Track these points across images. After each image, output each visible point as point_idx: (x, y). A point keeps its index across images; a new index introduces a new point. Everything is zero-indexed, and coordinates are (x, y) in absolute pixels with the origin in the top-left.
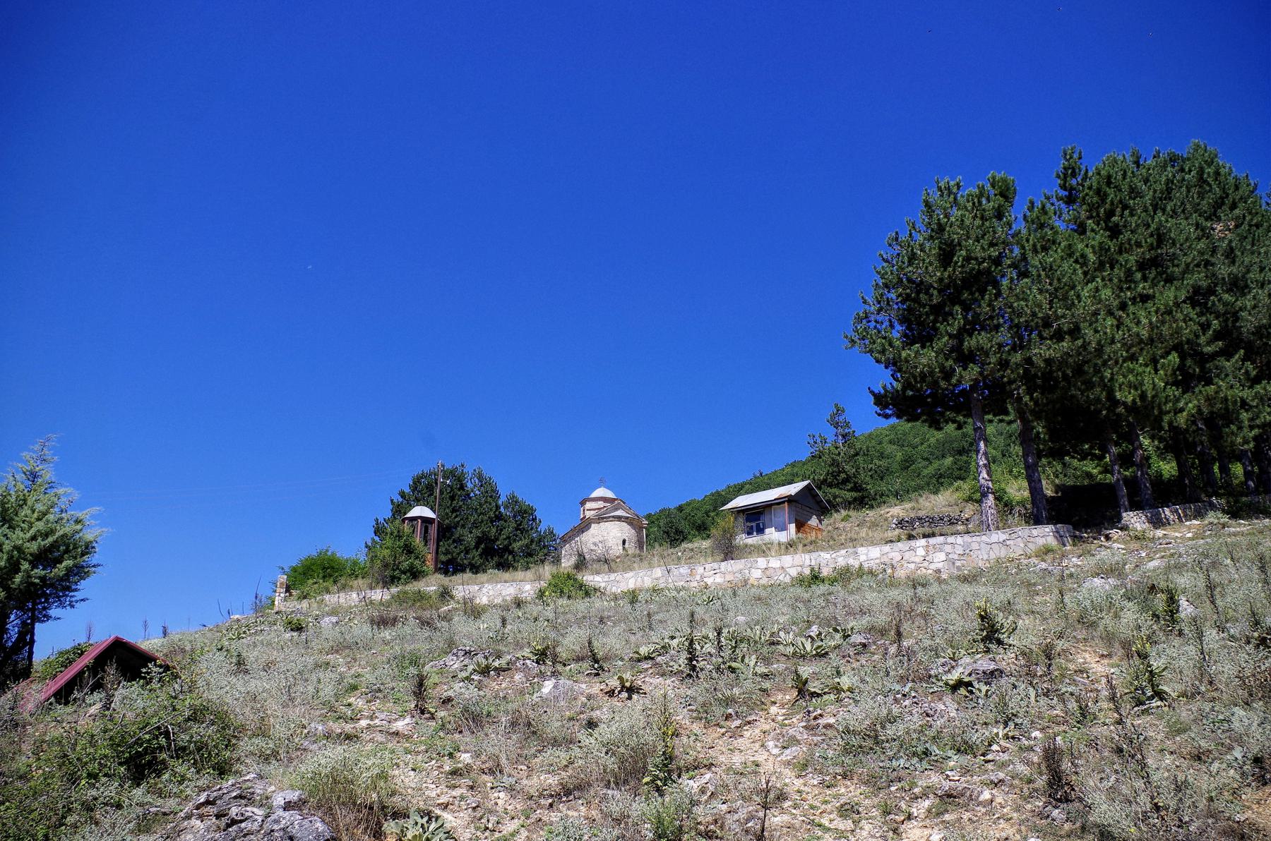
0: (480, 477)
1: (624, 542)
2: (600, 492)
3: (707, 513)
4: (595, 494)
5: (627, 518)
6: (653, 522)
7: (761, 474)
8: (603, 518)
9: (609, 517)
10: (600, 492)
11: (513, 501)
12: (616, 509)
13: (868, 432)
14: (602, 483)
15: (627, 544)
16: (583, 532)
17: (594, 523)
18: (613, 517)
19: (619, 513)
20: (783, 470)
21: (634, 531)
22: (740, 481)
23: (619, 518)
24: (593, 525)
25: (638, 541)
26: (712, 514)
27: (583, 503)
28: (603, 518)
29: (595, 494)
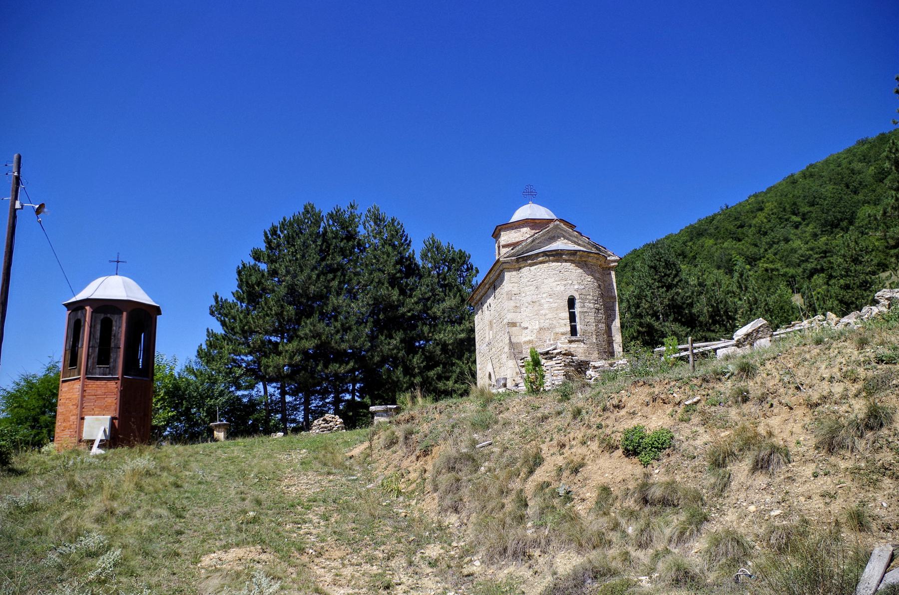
0: (378, 219)
1: (571, 302)
2: (524, 212)
3: (685, 243)
4: (521, 214)
5: (574, 253)
6: (639, 256)
7: (727, 207)
8: (526, 259)
9: (537, 255)
10: (524, 212)
11: (434, 247)
12: (553, 239)
13: (824, 158)
14: (530, 196)
15: (578, 305)
16: (495, 288)
17: (509, 270)
18: (545, 254)
19: (560, 245)
20: (747, 201)
21: (590, 278)
22: (711, 214)
23: (557, 255)
24: (507, 275)
25: (602, 296)
26: (690, 244)
27: (496, 235)
28: (529, 257)
29: (521, 214)
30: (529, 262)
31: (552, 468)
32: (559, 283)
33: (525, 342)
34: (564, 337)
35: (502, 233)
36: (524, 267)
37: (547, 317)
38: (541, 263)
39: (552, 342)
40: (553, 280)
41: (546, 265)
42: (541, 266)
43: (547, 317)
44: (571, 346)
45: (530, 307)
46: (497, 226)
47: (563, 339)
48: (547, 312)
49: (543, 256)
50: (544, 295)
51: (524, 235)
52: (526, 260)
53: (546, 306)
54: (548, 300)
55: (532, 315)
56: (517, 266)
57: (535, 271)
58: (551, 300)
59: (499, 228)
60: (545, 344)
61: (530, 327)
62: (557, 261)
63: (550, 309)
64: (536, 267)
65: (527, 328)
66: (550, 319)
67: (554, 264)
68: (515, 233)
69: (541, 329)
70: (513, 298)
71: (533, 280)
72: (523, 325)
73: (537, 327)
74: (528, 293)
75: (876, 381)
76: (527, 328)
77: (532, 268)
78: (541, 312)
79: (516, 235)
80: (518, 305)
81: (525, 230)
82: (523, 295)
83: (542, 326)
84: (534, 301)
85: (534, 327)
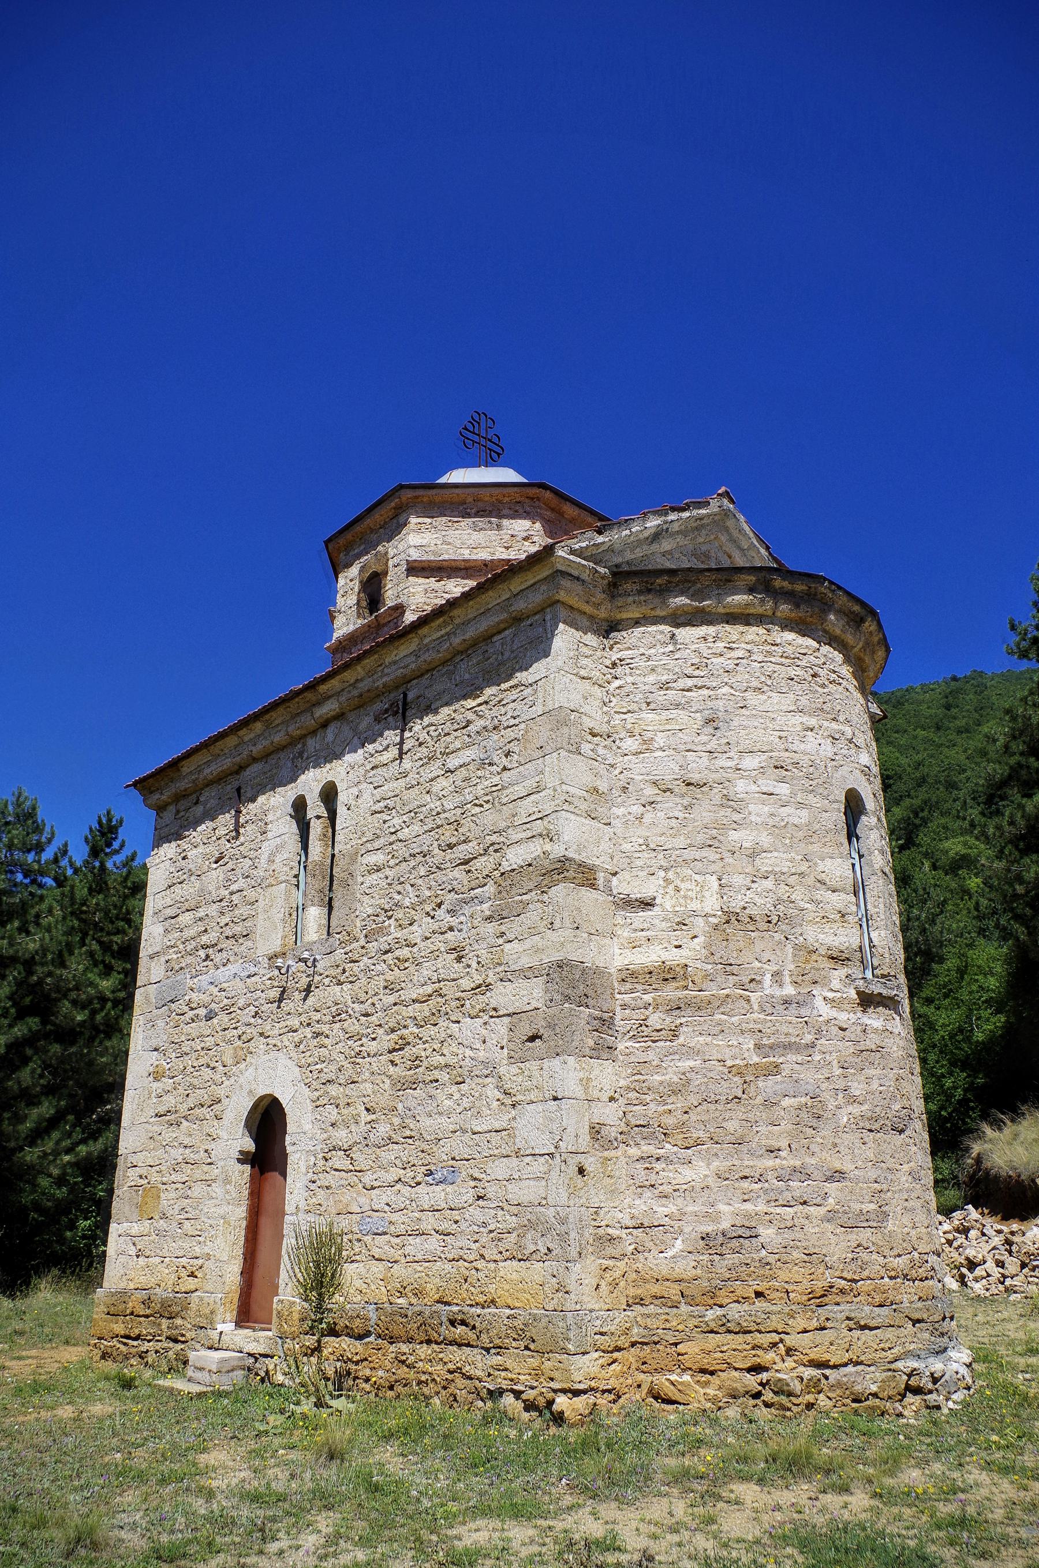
30: (681, 600)
31: (700, 1548)
32: (813, 722)
33: (630, 975)
34: (842, 972)
35: (413, 520)
36: (637, 623)
37: (765, 863)
38: (732, 618)
39: (789, 990)
40: (787, 702)
41: (754, 632)
42: (733, 631)
43: (765, 863)
44: (866, 1020)
45: (671, 805)
46: (402, 487)
47: (836, 984)
48: (765, 840)
49: (751, 590)
50: (750, 762)
51: (517, 546)
52: (664, 592)
53: (759, 811)
54: (767, 784)
55: (681, 842)
56: (603, 614)
57: (702, 646)
58: (784, 789)
59: (408, 494)
60: (754, 997)
61: (666, 903)
62: (802, 628)
63: (779, 829)
64: (710, 630)
65: (647, 904)
66: (779, 877)
67: (789, 636)
68: (476, 528)
69: (730, 917)
70: (586, 748)
71: (690, 683)
72: (622, 886)
73: (711, 903)
74: (660, 740)
75: (634, 1275)
76: (647, 904)
77: (685, 634)
78: (733, 835)
79: (477, 537)
80: (603, 787)
81: (521, 526)
82: (630, 744)
83: (736, 905)
84: (695, 777)
85: (694, 905)
